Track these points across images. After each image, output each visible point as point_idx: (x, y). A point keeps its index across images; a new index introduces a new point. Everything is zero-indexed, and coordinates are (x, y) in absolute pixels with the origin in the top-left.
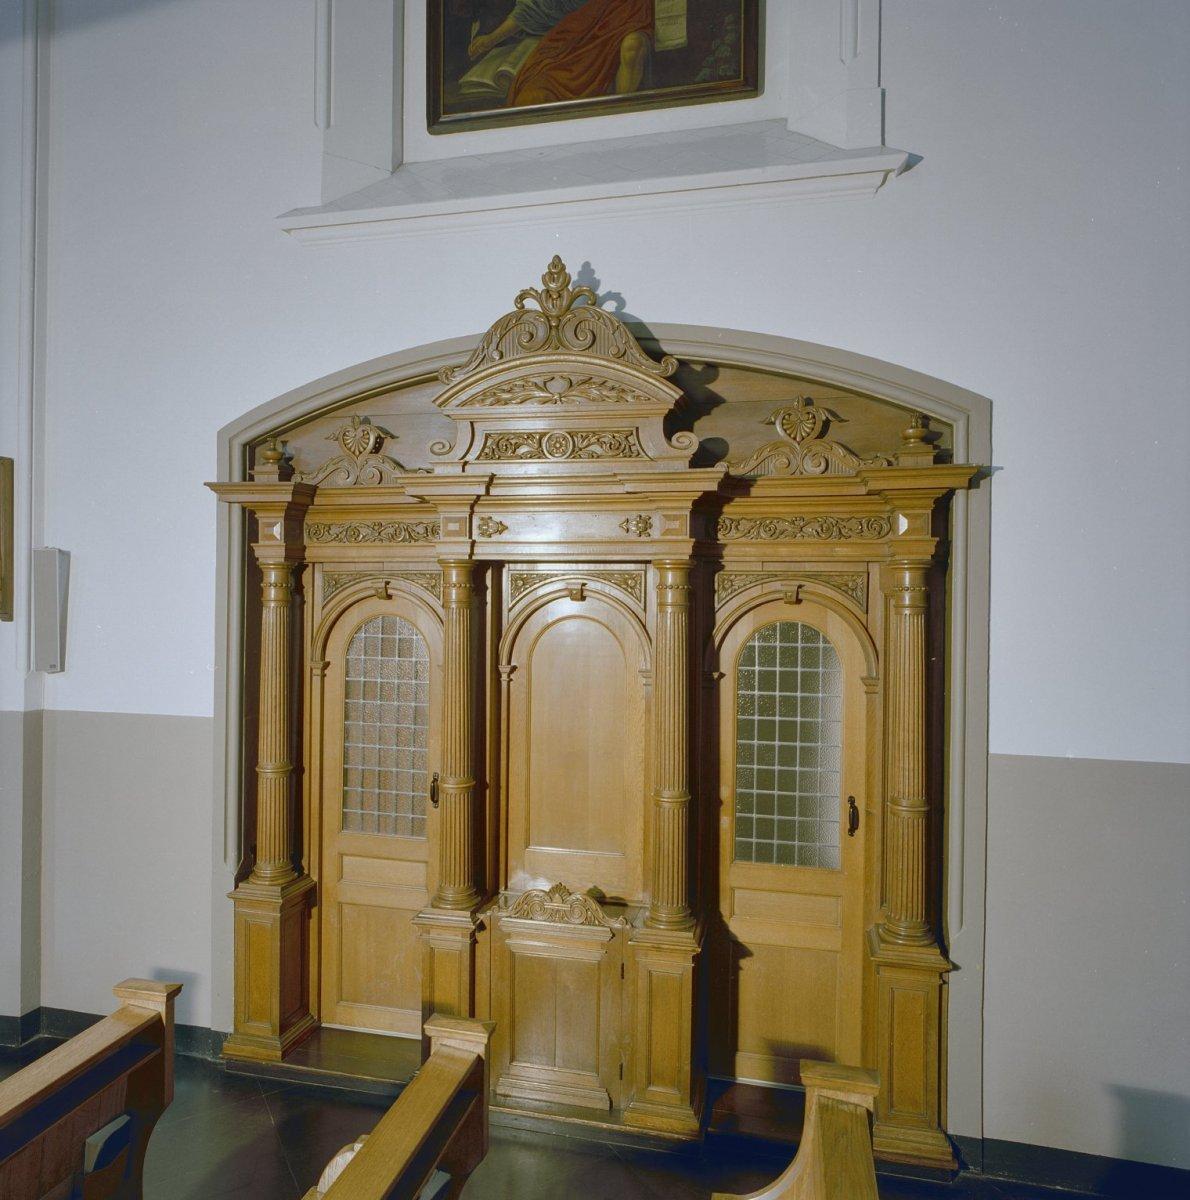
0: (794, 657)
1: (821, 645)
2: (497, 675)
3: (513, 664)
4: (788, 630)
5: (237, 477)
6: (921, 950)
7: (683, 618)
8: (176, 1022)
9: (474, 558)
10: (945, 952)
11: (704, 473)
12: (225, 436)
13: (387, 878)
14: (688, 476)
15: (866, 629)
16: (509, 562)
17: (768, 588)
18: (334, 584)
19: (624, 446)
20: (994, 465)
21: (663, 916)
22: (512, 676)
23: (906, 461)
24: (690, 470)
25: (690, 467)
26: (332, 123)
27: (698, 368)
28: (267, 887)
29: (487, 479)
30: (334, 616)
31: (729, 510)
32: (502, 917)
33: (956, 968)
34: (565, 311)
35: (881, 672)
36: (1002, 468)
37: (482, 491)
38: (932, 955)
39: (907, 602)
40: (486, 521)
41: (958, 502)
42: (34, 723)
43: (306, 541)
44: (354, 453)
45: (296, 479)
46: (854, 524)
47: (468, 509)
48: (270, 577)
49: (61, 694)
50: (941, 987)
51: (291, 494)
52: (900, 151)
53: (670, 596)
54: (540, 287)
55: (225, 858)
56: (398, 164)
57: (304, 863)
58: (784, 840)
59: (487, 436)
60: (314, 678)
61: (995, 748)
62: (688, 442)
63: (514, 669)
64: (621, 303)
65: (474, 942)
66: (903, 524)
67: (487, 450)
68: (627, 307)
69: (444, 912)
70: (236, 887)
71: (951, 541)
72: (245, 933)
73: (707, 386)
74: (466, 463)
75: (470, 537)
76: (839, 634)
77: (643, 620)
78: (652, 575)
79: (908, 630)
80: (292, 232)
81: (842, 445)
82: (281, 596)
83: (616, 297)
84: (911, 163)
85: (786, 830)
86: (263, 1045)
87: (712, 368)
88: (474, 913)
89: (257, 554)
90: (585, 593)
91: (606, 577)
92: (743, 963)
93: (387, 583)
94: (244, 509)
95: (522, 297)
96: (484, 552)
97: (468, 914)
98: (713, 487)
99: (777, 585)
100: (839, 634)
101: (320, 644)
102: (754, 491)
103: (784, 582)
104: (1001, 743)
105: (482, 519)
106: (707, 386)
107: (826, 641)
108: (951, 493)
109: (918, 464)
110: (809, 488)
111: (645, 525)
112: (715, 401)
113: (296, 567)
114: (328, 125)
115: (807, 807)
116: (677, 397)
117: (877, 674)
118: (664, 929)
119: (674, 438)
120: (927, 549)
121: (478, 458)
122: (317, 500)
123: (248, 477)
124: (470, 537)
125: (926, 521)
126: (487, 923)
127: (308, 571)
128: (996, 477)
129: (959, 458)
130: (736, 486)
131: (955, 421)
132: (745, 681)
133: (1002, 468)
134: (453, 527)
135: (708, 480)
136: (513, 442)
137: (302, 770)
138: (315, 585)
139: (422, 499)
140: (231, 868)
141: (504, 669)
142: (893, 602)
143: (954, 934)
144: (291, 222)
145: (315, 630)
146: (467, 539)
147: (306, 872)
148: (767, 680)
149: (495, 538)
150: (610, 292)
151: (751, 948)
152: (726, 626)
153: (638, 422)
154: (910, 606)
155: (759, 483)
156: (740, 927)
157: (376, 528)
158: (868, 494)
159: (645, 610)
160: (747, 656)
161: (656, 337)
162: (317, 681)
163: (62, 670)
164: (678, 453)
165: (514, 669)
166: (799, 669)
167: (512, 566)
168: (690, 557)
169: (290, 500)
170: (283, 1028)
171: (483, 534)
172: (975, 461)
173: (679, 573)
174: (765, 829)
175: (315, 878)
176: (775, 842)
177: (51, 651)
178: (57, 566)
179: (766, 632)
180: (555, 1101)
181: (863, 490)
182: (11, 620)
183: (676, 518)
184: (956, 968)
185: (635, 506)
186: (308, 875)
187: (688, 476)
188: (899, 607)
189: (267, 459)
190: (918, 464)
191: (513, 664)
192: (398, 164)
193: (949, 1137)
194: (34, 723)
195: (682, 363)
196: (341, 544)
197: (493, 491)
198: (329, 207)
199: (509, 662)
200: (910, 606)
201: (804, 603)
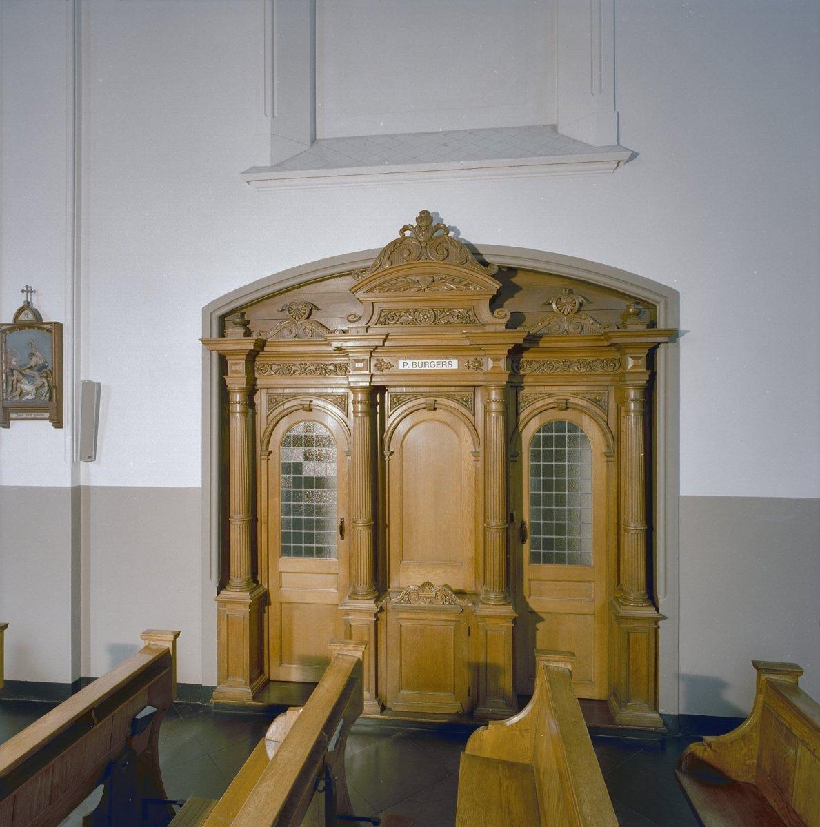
0: (558, 439)
1: (579, 434)
2: (383, 456)
3: (391, 450)
4: (560, 426)
5: (215, 336)
6: (645, 609)
7: (641, 418)
8: (178, 681)
9: (372, 384)
10: (657, 610)
11: (509, 332)
12: (207, 311)
13: (312, 586)
14: (244, 341)
15: (474, 426)
16: (390, 387)
17: (418, 401)
18: (273, 402)
19: (468, 319)
20: (682, 328)
21: (492, 596)
22: (270, 457)
23: (631, 327)
24: (245, 338)
25: (245, 336)
26: (276, 115)
27: (505, 270)
28: (239, 596)
29: (384, 337)
30: (274, 422)
31: (526, 356)
32: (393, 600)
33: (665, 618)
34: (429, 234)
35: (616, 449)
36: (689, 331)
37: (381, 344)
38: (649, 612)
39: (632, 408)
40: (380, 361)
41: (661, 351)
42: (78, 494)
43: (256, 375)
44: (563, 313)
45: (254, 336)
46: (332, 368)
47: (369, 354)
48: (492, 395)
49: (97, 475)
50: (656, 629)
51: (249, 343)
52: (628, 150)
53: (360, 407)
54: (415, 224)
55: (210, 577)
56: (314, 140)
57: (259, 579)
58: (555, 549)
59: (382, 311)
60: (263, 461)
61: (682, 494)
62: (505, 313)
63: (392, 453)
64: (458, 233)
65: (377, 619)
66: (631, 363)
67: (381, 320)
68: (461, 233)
69: (356, 601)
70: (219, 593)
71: (656, 373)
72: (225, 621)
73: (512, 280)
74: (369, 327)
75: (370, 372)
76: (591, 429)
77: (473, 421)
78: (351, 395)
79: (632, 425)
80: (251, 183)
81: (591, 317)
82: (365, 410)
83: (454, 229)
84: (634, 156)
85: (309, 538)
86: (239, 692)
87: (512, 270)
88: (376, 602)
89: (227, 383)
90: (311, 407)
91: (448, 396)
92: (538, 625)
93: (311, 402)
94: (220, 355)
95: (405, 228)
96: (378, 381)
97: (373, 602)
98: (252, 347)
99: (422, 400)
100: (591, 429)
101: (265, 441)
102: (542, 344)
103: (427, 398)
104: (688, 487)
105: (378, 360)
106: (512, 280)
107: (582, 431)
108: (659, 344)
109: (628, 332)
110: (578, 342)
111: (479, 365)
112: (517, 288)
113: (251, 392)
114: (274, 116)
115: (320, 525)
116: (498, 287)
117: (614, 450)
118: (633, 606)
119: (495, 314)
120: (643, 379)
121: (376, 324)
122: (266, 349)
123: (222, 334)
124: (370, 372)
125: (642, 362)
126: (384, 607)
127: (258, 393)
128: (682, 340)
129: (661, 325)
130: (533, 339)
131: (658, 303)
132: (535, 456)
133: (689, 331)
134: (360, 365)
135: (517, 337)
136: (398, 314)
137: (257, 520)
138: (261, 399)
139: (340, 349)
140: (214, 583)
141: (386, 453)
142: (623, 409)
143: (661, 599)
144: (249, 177)
145: (262, 434)
146: (368, 372)
147: (260, 583)
148: (548, 455)
149: (386, 371)
150: (456, 227)
151: (543, 616)
152: (524, 422)
153: (475, 303)
154: (362, 412)
155: (544, 339)
156: (534, 603)
157: (303, 366)
158: (609, 346)
159: (474, 415)
160: (535, 441)
161: (481, 253)
162: (264, 463)
163: (95, 459)
164: (500, 321)
165: (392, 453)
166: (554, 449)
167: (393, 390)
168: (647, 382)
169: (252, 348)
170: (251, 681)
171: (378, 370)
172: (670, 327)
173: (364, 394)
174: (298, 538)
175: (266, 587)
176: (303, 545)
177: (87, 449)
178: (92, 394)
179: (547, 427)
180: (451, 712)
181: (606, 343)
182: (62, 427)
183: (640, 358)
184: (665, 618)
185: (473, 353)
186: (261, 585)
187: (244, 341)
188: (628, 411)
189: (236, 323)
190: (628, 332)
191: (270, 450)
192: (314, 140)
193: (661, 715)
194: (78, 494)
195: (500, 267)
196: (280, 376)
197: (386, 344)
198: (278, 166)
199: (388, 450)
200: (362, 412)
201: (313, 411)
